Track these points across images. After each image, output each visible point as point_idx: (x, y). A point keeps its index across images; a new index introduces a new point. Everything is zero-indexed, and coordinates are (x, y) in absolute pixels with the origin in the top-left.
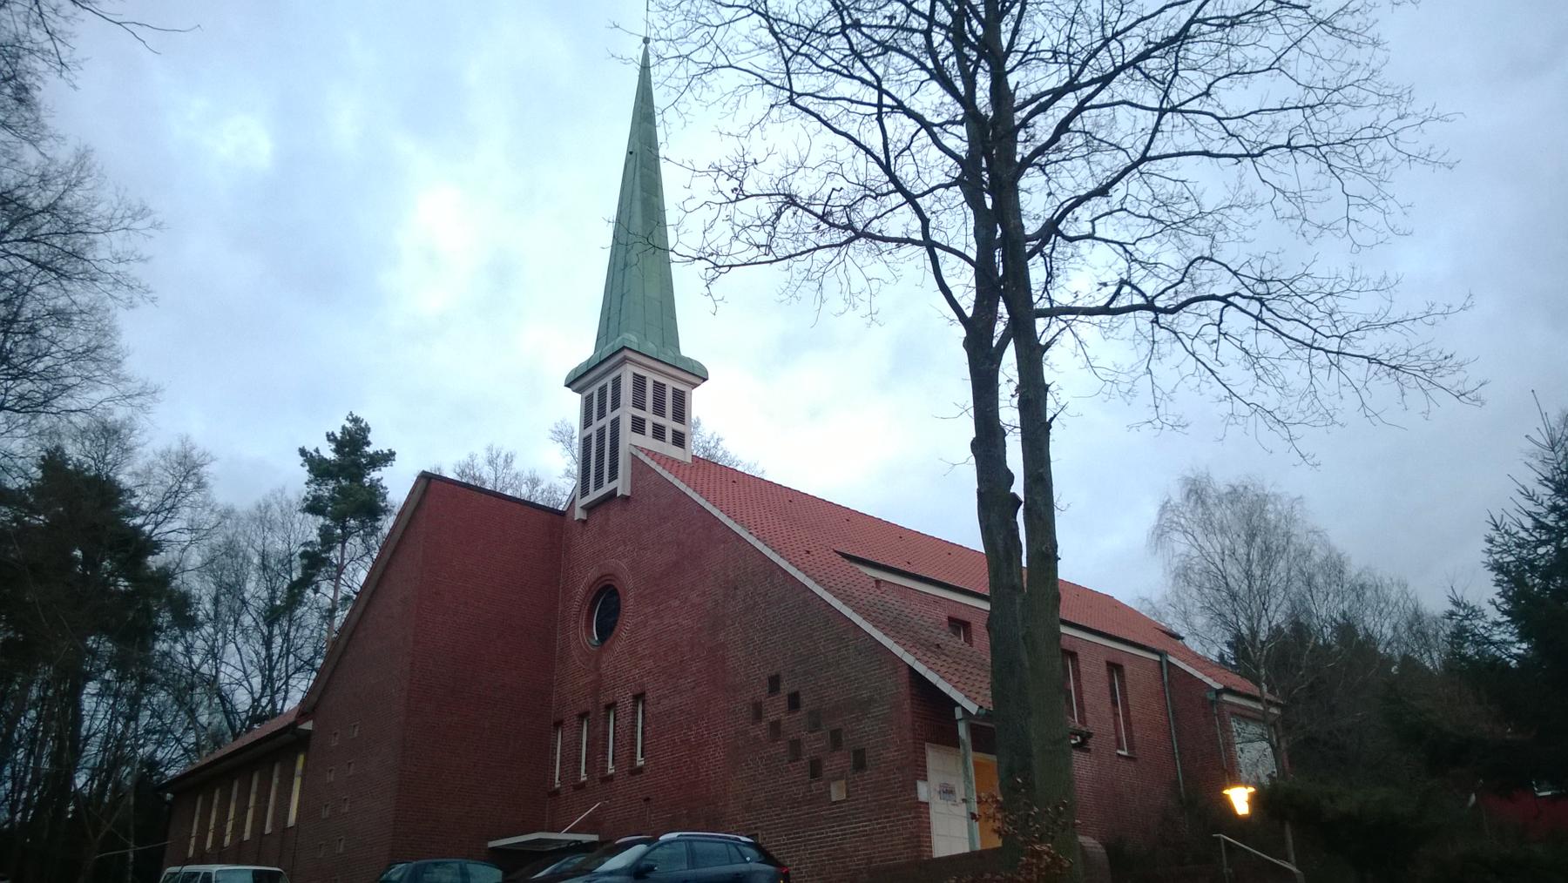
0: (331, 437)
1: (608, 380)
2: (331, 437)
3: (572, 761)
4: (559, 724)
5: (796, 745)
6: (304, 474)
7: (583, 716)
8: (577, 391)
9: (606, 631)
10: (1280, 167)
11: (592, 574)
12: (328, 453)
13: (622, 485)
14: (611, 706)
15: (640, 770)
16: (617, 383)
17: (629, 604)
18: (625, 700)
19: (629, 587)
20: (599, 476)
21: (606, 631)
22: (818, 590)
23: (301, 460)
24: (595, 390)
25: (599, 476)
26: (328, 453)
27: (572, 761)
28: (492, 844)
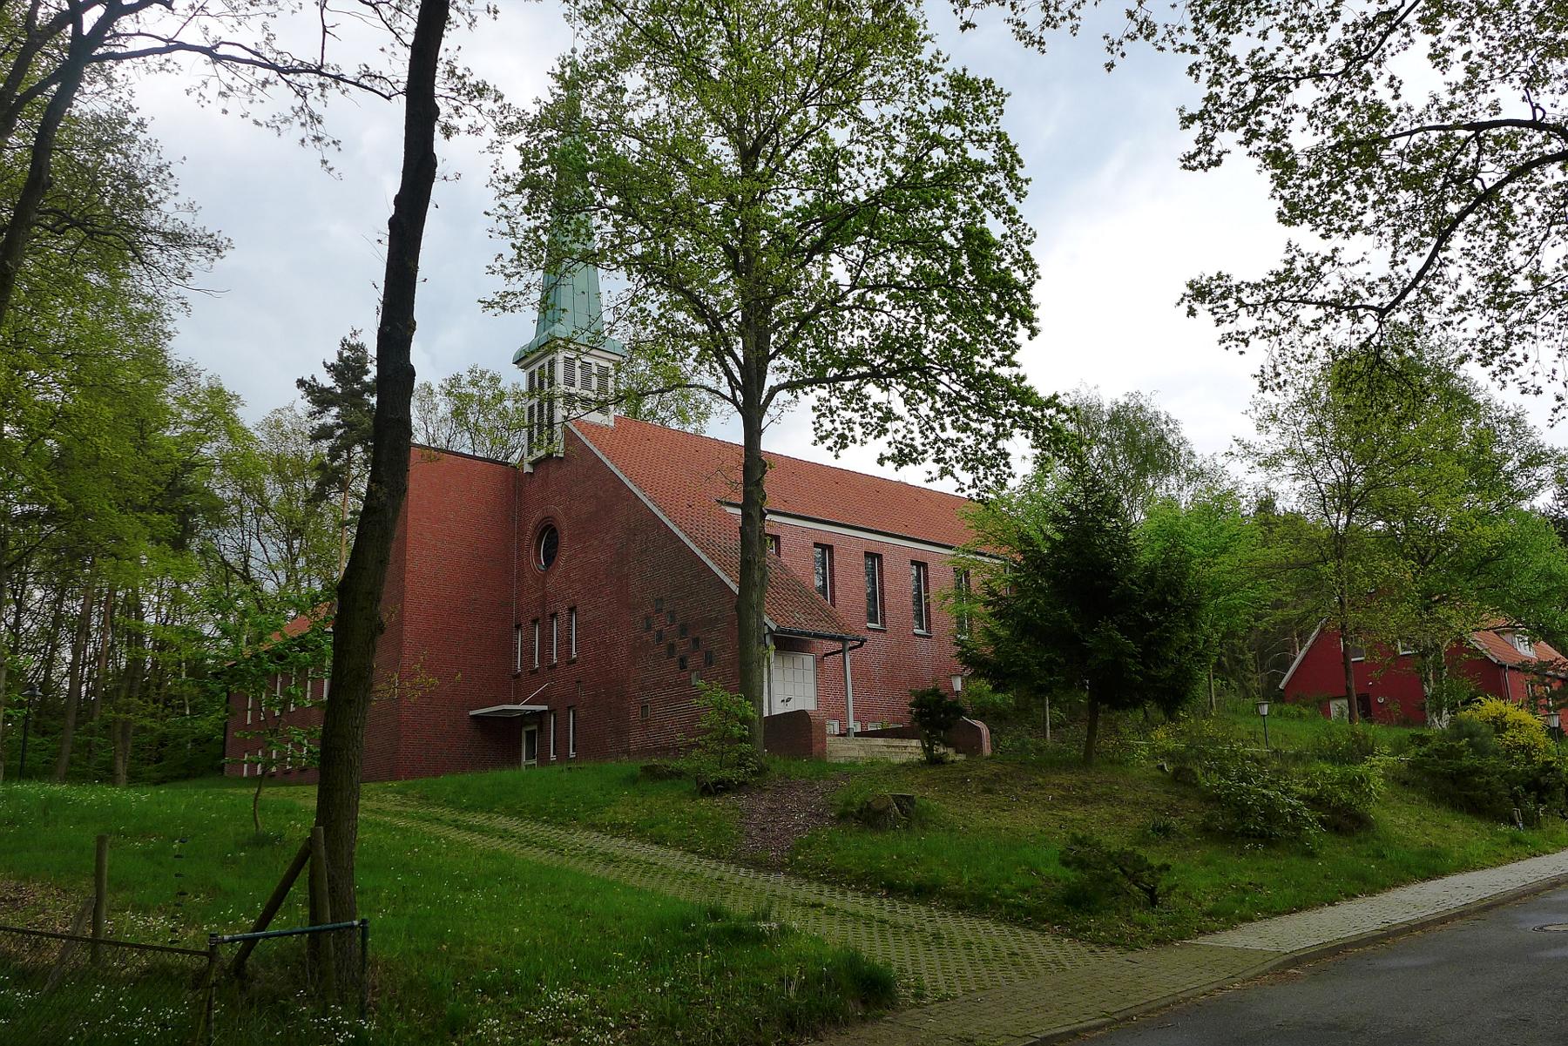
0: (331, 368)
1: (545, 361)
2: (331, 368)
3: (528, 653)
4: (518, 627)
5: (672, 647)
6: (303, 405)
7: (535, 621)
8: (525, 367)
9: (550, 558)
10: (1137, 959)
11: (538, 515)
12: (327, 381)
13: (559, 449)
14: (553, 616)
15: (574, 661)
16: (552, 364)
17: (564, 541)
18: (563, 612)
19: (564, 526)
20: (541, 384)
21: (550, 558)
22: (687, 541)
23: (301, 392)
24: (535, 367)
25: (541, 384)
26: (327, 381)
27: (528, 653)
28: (472, 713)
